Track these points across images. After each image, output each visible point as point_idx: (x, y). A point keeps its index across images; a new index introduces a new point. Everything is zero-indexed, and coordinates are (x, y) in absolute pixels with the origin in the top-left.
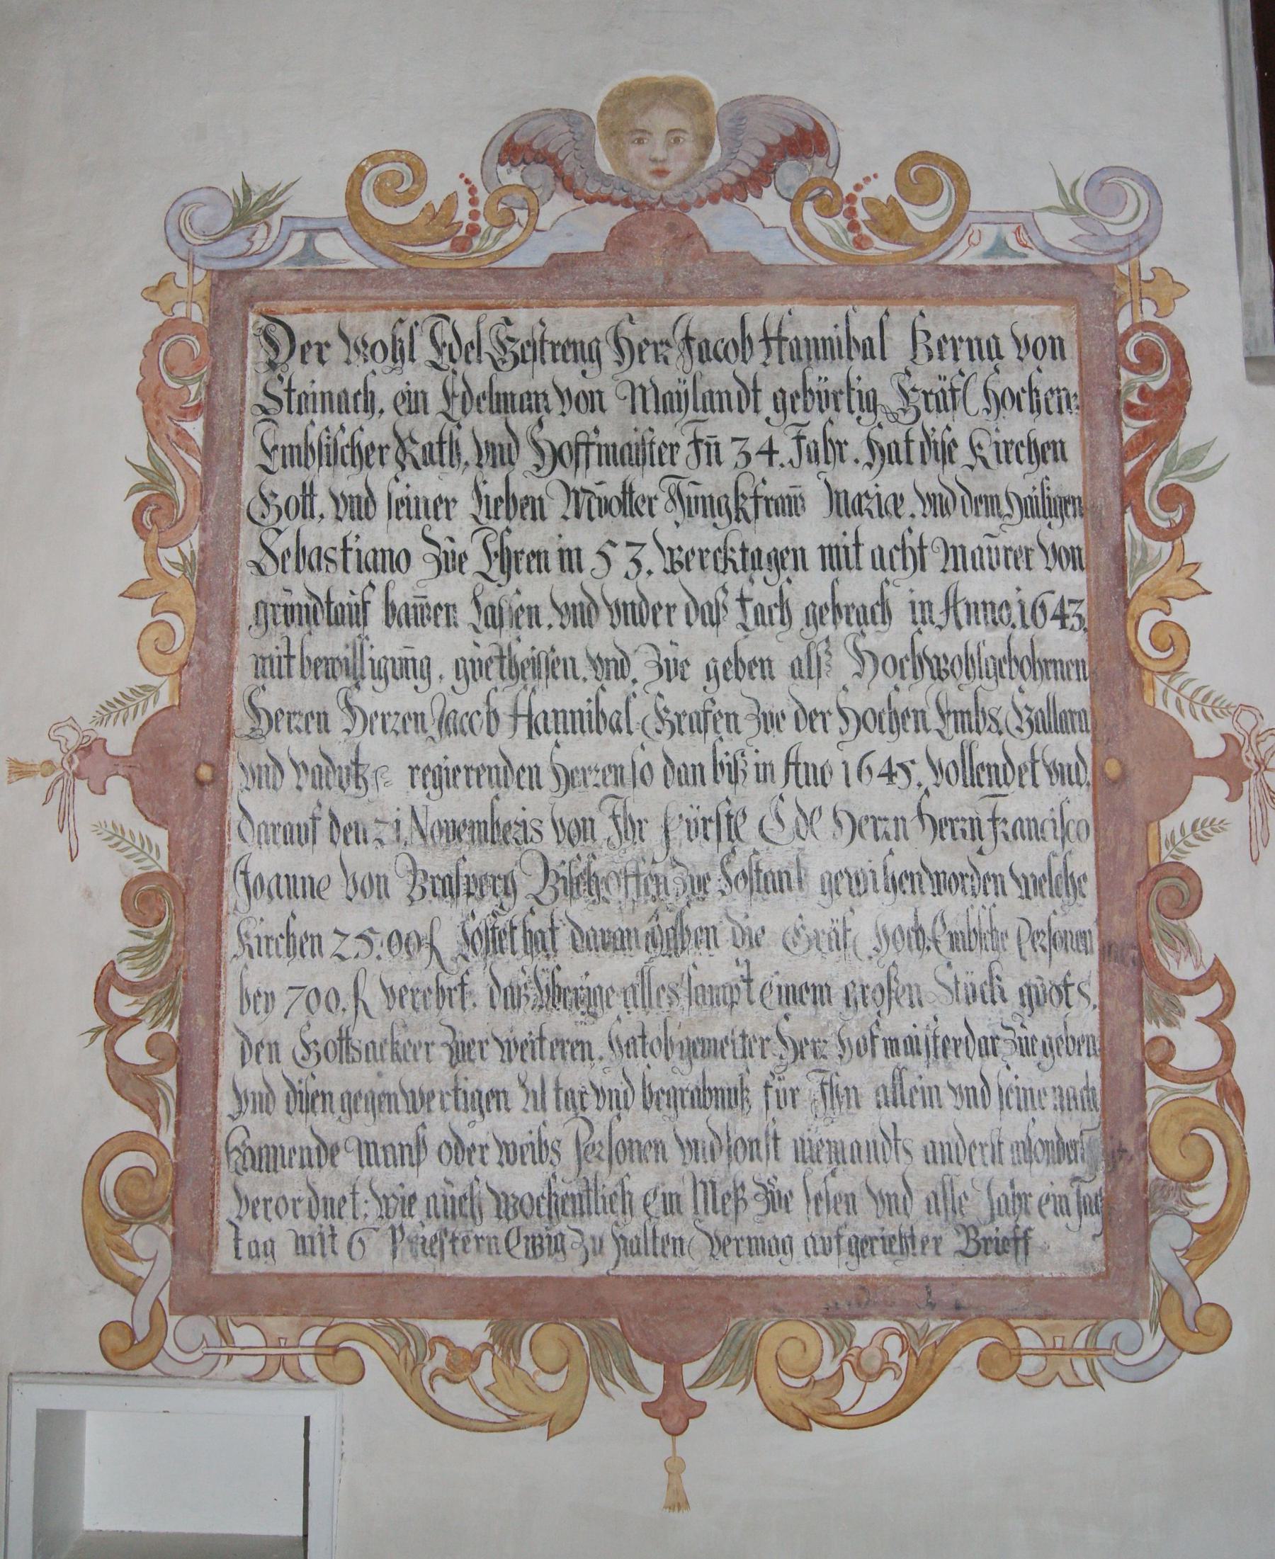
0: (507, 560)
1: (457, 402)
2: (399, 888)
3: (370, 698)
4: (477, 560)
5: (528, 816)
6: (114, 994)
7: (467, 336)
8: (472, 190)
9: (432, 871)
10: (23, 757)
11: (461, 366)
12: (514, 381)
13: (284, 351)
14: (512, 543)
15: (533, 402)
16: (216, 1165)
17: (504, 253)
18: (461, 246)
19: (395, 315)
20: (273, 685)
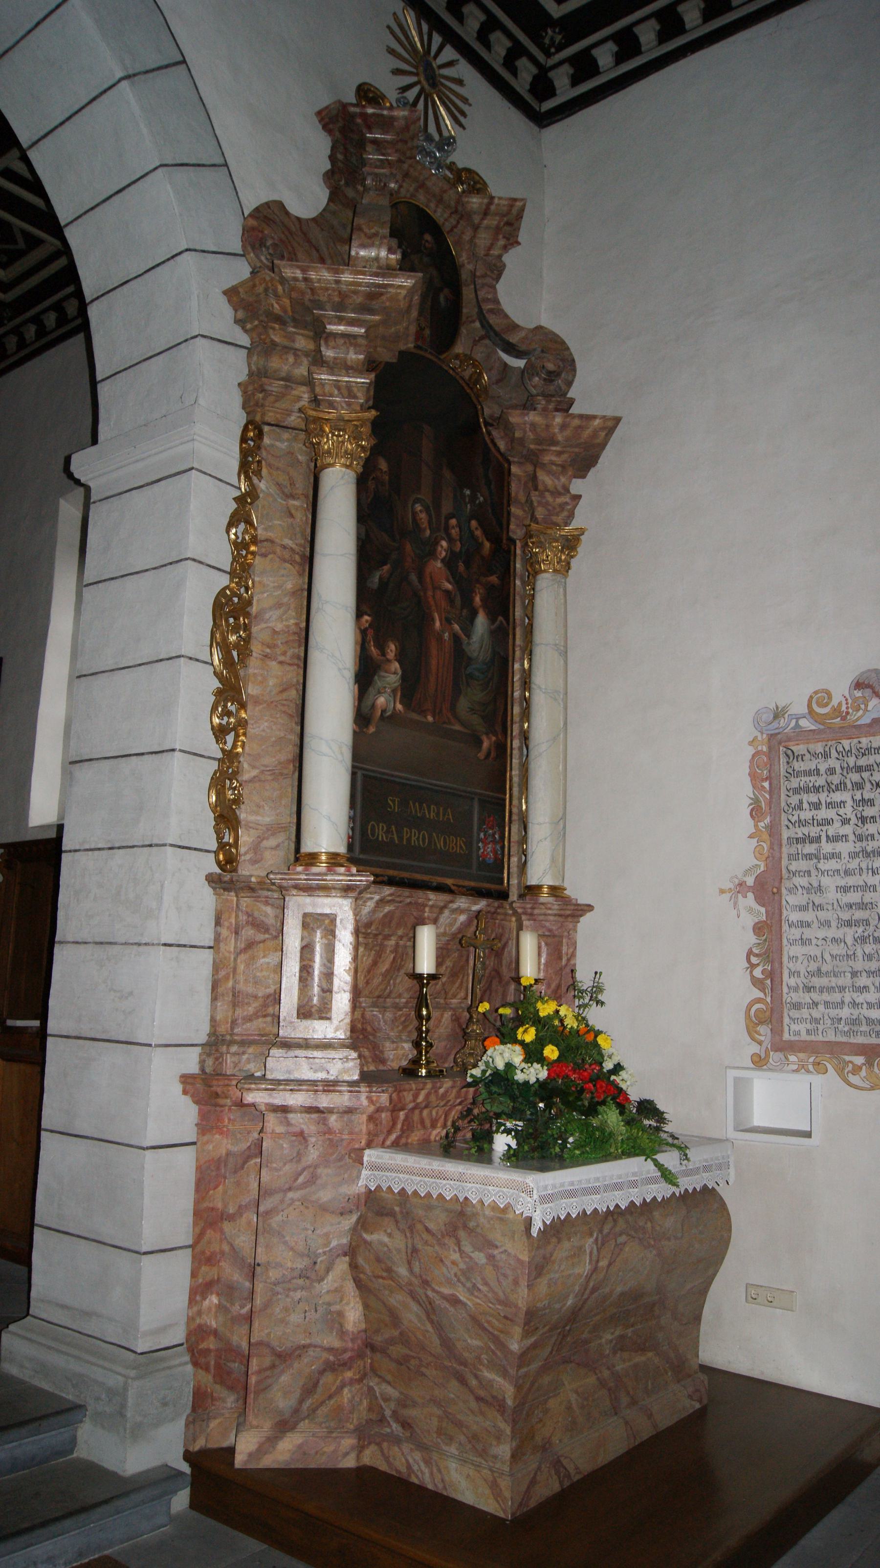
0: (863, 820)
1: (845, 770)
2: (834, 924)
3: (824, 865)
4: (854, 820)
5: (873, 901)
6: (752, 957)
7: (847, 748)
8: (846, 700)
9: (844, 918)
10: (723, 888)
11: (846, 758)
12: (862, 762)
13: (791, 758)
14: (865, 814)
15: (869, 768)
16: (783, 1008)
17: (857, 720)
18: (844, 719)
19: (824, 743)
20: (794, 863)
